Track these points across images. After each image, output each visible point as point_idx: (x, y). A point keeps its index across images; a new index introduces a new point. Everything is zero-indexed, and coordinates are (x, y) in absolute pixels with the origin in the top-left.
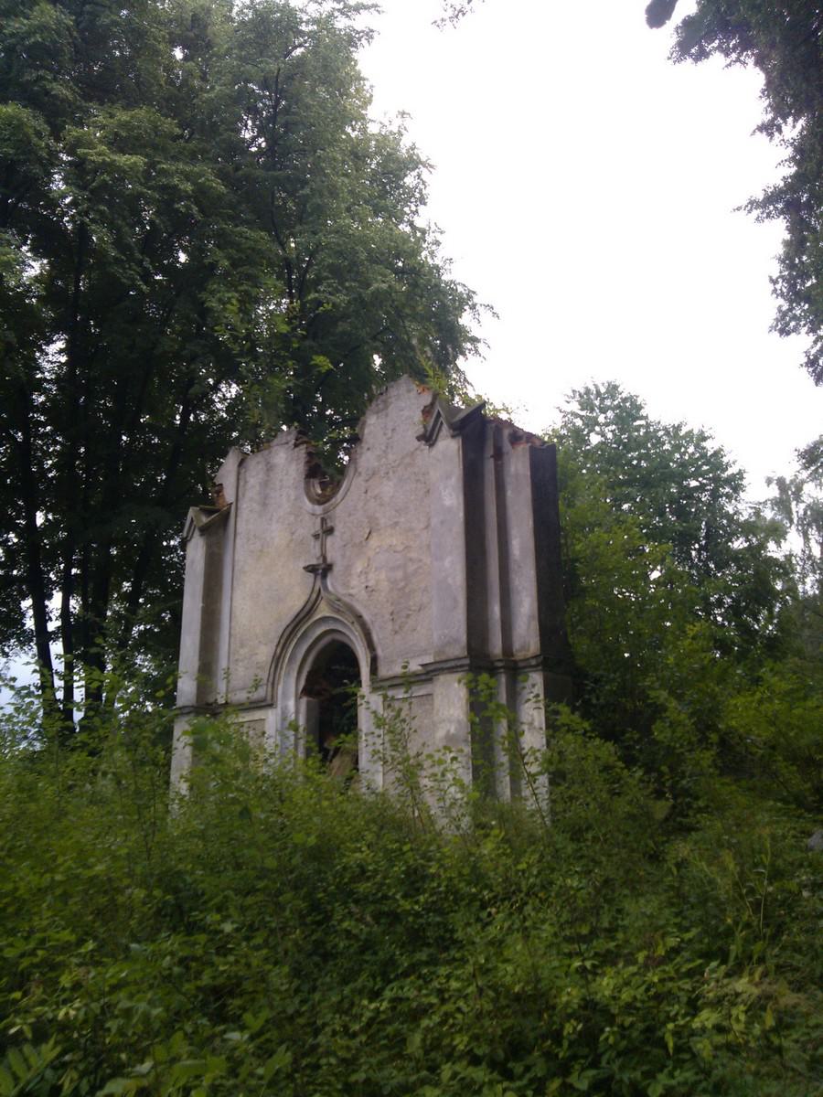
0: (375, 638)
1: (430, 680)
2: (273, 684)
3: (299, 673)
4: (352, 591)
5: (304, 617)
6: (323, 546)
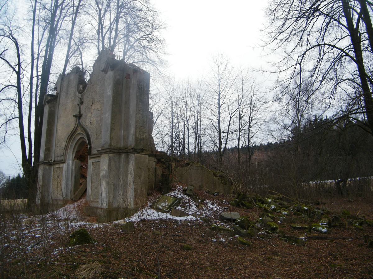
1: (100, 157)
2: (65, 155)
3: (73, 151)
5: (74, 133)
6: (80, 108)
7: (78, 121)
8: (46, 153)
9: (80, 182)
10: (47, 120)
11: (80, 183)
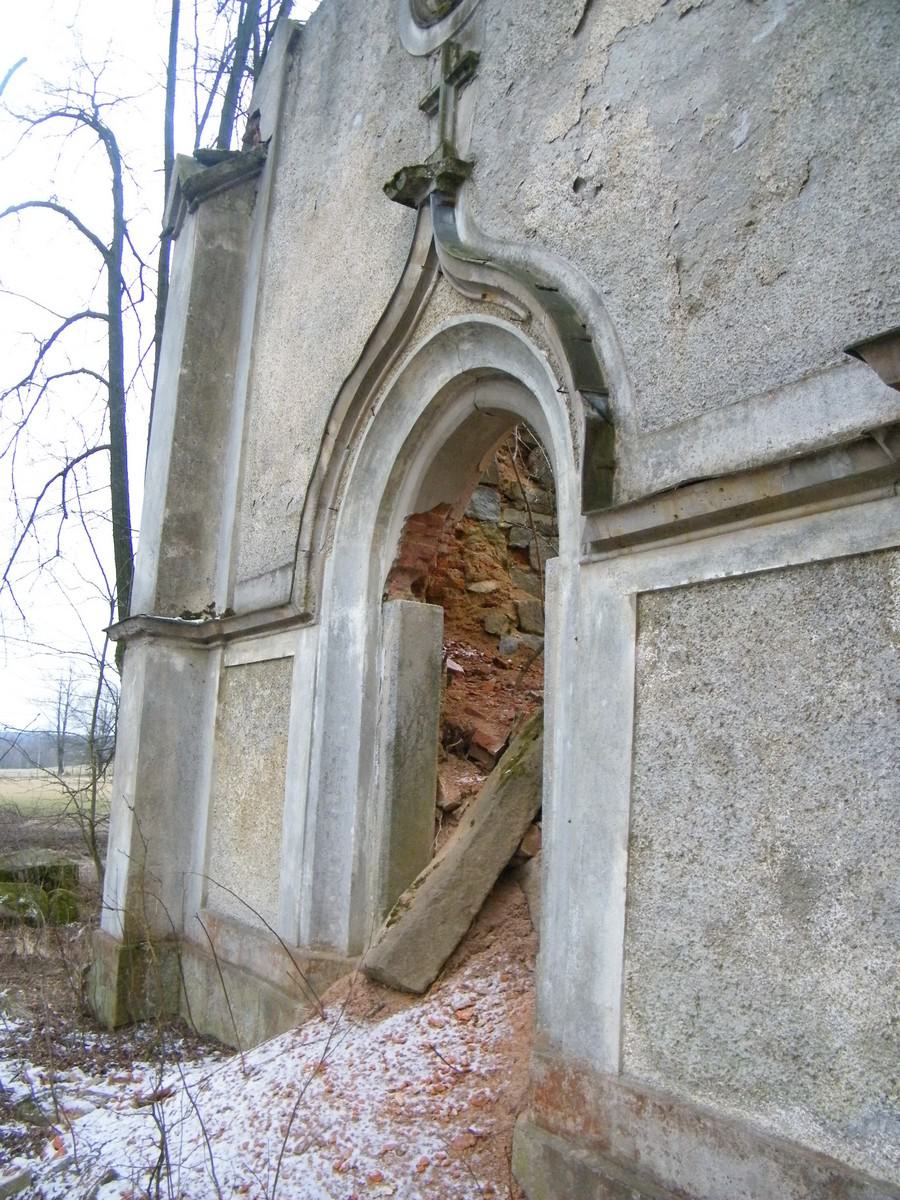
0: (606, 349)
2: (310, 556)
3: (382, 520)
4: (531, 220)
7: (438, 221)
8: (172, 553)
9: (439, 794)
10: (184, 313)
11: (439, 807)
